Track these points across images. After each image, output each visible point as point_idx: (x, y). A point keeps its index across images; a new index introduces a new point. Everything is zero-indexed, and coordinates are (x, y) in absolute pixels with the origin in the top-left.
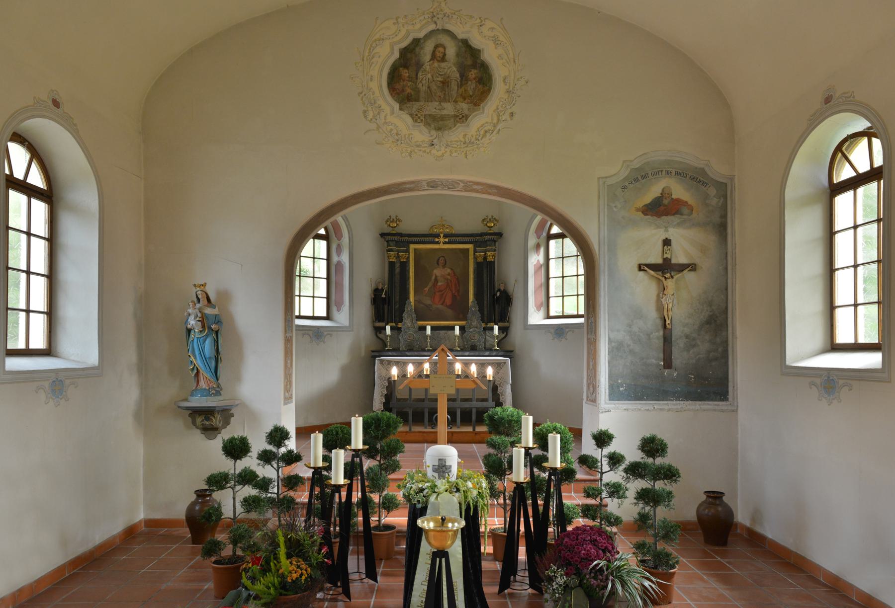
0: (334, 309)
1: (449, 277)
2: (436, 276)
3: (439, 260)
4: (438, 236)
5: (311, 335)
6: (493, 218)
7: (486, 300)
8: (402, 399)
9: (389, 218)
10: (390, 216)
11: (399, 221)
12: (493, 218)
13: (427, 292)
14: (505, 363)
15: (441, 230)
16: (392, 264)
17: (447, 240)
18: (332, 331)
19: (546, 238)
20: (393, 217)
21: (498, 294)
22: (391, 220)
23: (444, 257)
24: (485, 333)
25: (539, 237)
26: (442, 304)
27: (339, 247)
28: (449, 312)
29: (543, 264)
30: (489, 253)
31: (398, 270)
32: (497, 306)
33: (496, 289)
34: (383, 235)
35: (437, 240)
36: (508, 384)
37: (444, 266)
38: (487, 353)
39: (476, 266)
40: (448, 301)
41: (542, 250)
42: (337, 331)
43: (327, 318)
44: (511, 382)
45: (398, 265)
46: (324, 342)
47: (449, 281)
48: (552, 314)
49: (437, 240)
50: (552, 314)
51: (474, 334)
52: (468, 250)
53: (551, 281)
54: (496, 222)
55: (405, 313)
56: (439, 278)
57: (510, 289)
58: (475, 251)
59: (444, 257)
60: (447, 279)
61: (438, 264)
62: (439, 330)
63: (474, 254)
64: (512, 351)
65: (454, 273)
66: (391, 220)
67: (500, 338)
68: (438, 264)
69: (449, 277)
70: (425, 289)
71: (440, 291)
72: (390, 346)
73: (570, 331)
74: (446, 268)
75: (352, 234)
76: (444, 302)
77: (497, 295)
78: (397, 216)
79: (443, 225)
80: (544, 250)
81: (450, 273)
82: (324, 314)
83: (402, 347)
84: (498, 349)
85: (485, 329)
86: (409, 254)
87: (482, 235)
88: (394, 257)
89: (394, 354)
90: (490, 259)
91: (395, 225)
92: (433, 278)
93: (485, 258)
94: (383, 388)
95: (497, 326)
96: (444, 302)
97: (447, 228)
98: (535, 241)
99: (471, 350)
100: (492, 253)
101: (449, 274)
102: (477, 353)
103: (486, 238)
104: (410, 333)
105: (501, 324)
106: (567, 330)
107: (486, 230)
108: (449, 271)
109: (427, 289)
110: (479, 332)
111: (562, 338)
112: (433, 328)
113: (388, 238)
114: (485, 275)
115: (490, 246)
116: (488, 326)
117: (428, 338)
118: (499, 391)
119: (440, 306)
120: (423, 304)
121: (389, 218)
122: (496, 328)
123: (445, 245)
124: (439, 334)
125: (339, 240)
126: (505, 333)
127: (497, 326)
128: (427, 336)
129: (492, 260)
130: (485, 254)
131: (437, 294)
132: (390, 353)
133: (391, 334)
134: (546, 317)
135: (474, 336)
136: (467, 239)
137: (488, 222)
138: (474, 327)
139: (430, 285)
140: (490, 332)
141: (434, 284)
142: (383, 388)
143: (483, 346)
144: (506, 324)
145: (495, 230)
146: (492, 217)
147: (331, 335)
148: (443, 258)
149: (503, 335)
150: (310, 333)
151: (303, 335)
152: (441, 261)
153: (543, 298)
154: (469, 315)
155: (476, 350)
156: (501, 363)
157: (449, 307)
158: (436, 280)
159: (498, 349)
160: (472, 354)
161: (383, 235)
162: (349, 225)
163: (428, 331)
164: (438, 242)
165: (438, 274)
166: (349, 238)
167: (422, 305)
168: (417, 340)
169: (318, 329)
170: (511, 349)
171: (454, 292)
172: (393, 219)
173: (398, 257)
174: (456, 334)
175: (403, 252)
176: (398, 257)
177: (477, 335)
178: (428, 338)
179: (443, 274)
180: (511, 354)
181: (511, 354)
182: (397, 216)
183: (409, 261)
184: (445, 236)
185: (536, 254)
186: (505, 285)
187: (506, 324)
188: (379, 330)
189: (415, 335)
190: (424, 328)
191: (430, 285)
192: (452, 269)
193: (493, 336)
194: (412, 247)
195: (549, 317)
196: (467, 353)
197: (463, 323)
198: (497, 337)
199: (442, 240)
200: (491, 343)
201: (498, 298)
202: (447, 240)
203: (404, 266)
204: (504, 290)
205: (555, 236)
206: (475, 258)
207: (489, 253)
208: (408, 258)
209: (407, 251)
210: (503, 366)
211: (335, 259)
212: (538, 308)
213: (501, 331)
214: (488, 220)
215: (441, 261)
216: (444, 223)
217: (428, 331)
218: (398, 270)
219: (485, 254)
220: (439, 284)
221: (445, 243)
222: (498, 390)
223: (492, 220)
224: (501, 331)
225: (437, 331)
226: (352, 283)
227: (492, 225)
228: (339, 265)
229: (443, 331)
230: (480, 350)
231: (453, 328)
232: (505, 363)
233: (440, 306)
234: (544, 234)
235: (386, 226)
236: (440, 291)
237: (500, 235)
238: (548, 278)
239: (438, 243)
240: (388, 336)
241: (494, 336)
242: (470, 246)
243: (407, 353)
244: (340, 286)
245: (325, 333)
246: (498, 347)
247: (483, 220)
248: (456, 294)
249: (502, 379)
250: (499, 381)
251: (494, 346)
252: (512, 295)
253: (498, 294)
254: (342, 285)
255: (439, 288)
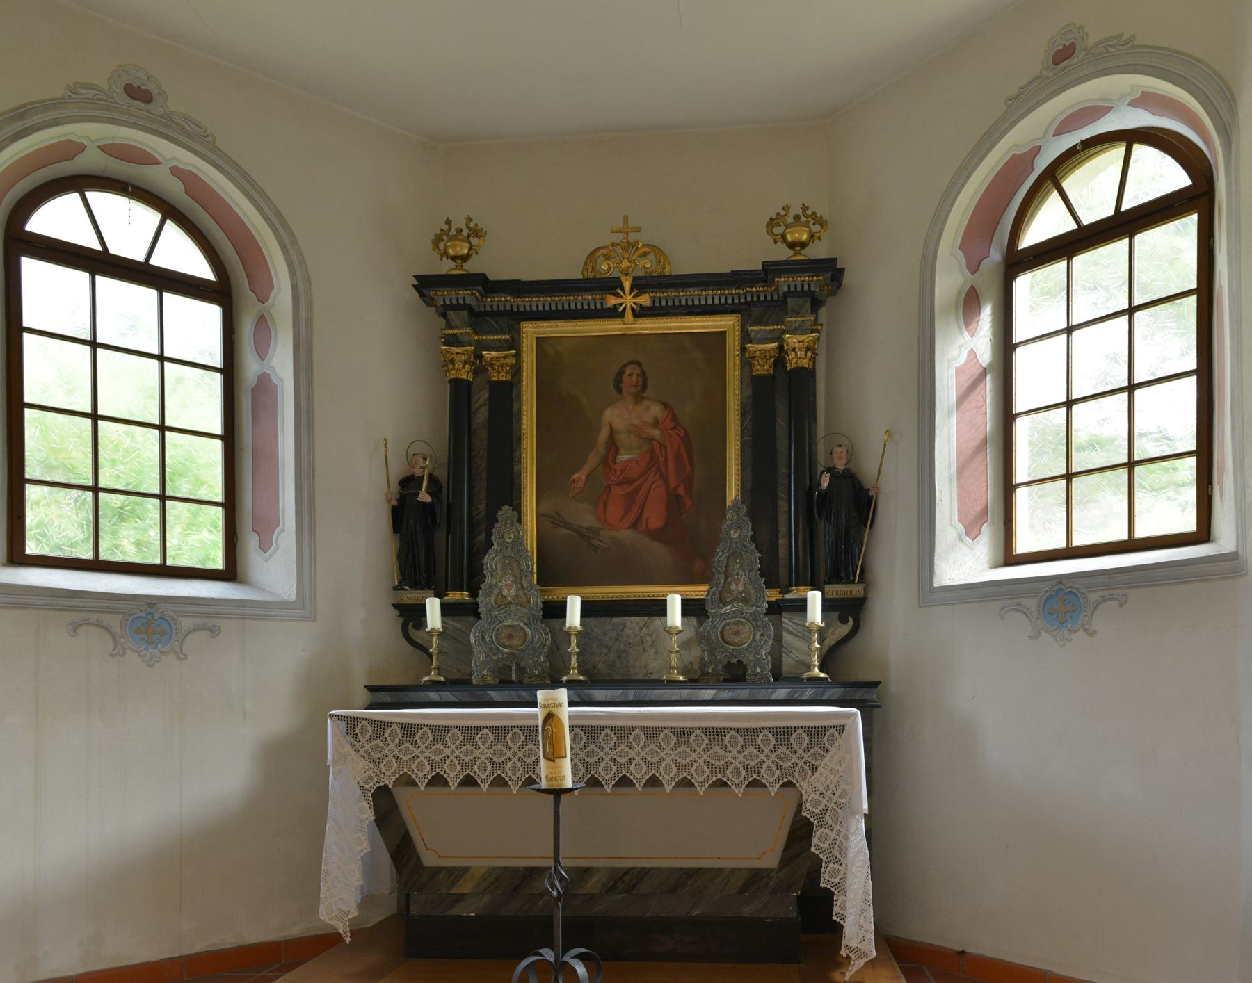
0: (250, 542)
1: (656, 433)
2: (612, 432)
3: (621, 373)
4: (612, 285)
5: (116, 628)
6: (809, 212)
7: (787, 507)
8: (442, 868)
9: (446, 227)
10: (448, 222)
11: (477, 232)
12: (809, 212)
13: (581, 484)
14: (841, 729)
15: (625, 264)
16: (460, 393)
17: (645, 300)
18: (219, 616)
19: (1002, 269)
20: (459, 223)
21: (825, 482)
22: (453, 232)
23: (638, 364)
24: (779, 628)
25: (974, 267)
26: (634, 526)
27: (263, 323)
28: (659, 552)
29: (991, 364)
30: (791, 340)
31: (481, 415)
32: (821, 525)
33: (820, 469)
34: (425, 284)
35: (611, 301)
36: (853, 814)
37: (639, 397)
38: (782, 693)
39: (749, 392)
40: (655, 517)
41: (986, 316)
42: (243, 617)
43: (230, 572)
44: (865, 806)
45: (481, 398)
46: (183, 657)
47: (656, 445)
48: (1022, 545)
49: (611, 301)
50: (1022, 545)
51: (737, 623)
52: (722, 335)
53: (1022, 427)
54: (816, 228)
55: (491, 551)
56: (621, 438)
57: (868, 469)
58: (746, 338)
59: (638, 364)
60: (650, 440)
61: (619, 390)
62: (622, 616)
63: (743, 349)
64: (875, 684)
65: (674, 418)
66: (453, 232)
67: (832, 639)
68: (619, 390)
69: (656, 433)
70: (576, 476)
71: (627, 481)
72: (438, 668)
73: (1111, 598)
74: (646, 403)
75: (308, 279)
76: (639, 518)
77: (820, 484)
78: (469, 219)
79: (630, 246)
80: (993, 314)
81: (660, 417)
82: (217, 562)
83: (480, 672)
84: (823, 675)
85: (776, 609)
86: (518, 356)
87: (771, 270)
88: (465, 363)
89: (448, 696)
90: (797, 359)
91: (465, 251)
92: (603, 435)
93: (780, 359)
94: (746, 767)
95: (818, 594)
96: (639, 518)
97: (644, 255)
98: (961, 280)
99: (726, 680)
100: (803, 337)
101: (656, 423)
102: (744, 693)
103: (784, 282)
104: (509, 622)
105: (837, 590)
106: (1094, 596)
107: (782, 253)
108: (656, 411)
109: (580, 476)
110: (755, 616)
111: (1071, 631)
112: (588, 609)
113: (445, 296)
114: (781, 423)
115: (797, 313)
116: (791, 596)
117: (574, 641)
118: (818, 843)
119: (626, 534)
120: (567, 525)
121: (446, 227)
122: (815, 599)
123: (640, 320)
124: (624, 626)
125: (262, 300)
126: (851, 622)
127: (818, 594)
128: (567, 635)
129: (805, 364)
130: (781, 348)
131: (618, 491)
132: (434, 696)
133: (443, 627)
134: (1002, 560)
135: (737, 633)
136: (712, 296)
137: (787, 226)
138: (736, 599)
139: (593, 460)
140: (797, 618)
141: (607, 457)
142: (746, 767)
143: (769, 667)
144: (854, 590)
145: (818, 251)
146: (805, 208)
147: (214, 631)
148: (637, 370)
149: (844, 630)
150: (109, 619)
151: (75, 627)
152: (631, 377)
153: (988, 490)
154: (721, 556)
155: (745, 681)
156: (825, 729)
157: (656, 535)
158: (613, 446)
159: (823, 675)
160: (726, 695)
161: (425, 284)
162: (294, 242)
163: (574, 617)
164: (615, 307)
165: (619, 424)
166: (295, 289)
167: (565, 531)
168: (535, 650)
169: (151, 605)
170: (872, 678)
171: (673, 484)
172: (460, 231)
173: (479, 366)
174: (669, 624)
175: (497, 350)
176: (479, 366)
177: (747, 629)
178: (574, 641)
179: (635, 421)
180: (872, 695)
181: (872, 695)
182: (469, 219)
183: (520, 382)
184: (641, 285)
185: (966, 334)
186: (851, 454)
187: (854, 590)
188: (413, 615)
189: (528, 631)
190: (556, 610)
191: (593, 460)
192: (666, 406)
193: (805, 632)
194: (530, 331)
195: (1011, 559)
196: (708, 694)
197: (699, 590)
198: (821, 631)
199: (629, 300)
200: (801, 657)
201: (824, 496)
202: (645, 300)
203: (505, 395)
204: (847, 470)
205: (1035, 257)
206: (746, 362)
207: (791, 340)
208: (517, 370)
209: (514, 344)
210: (833, 740)
211: (251, 367)
212: (972, 529)
213: (836, 615)
214: (790, 219)
215: (631, 377)
216: (633, 237)
217: (574, 617)
218: (481, 415)
219: (781, 348)
220: (624, 457)
221: (641, 313)
222: (815, 841)
223: (803, 219)
224: (836, 615)
225: (616, 620)
226: (311, 448)
227: (805, 237)
228: (265, 385)
229: (638, 619)
230: (758, 682)
231: (659, 608)
232: (841, 729)
233: (626, 534)
234: (996, 255)
235: (436, 256)
236: (627, 481)
237: (832, 271)
238: (1007, 417)
239: (614, 313)
240: (430, 633)
241: (810, 631)
242: (727, 323)
243: (495, 695)
244: (267, 457)
245: (186, 623)
246: (821, 670)
247: (772, 223)
248: (681, 491)
249: (828, 795)
250: (815, 803)
251: (809, 667)
252: (876, 486)
253: (825, 482)
254: (273, 458)
255: (622, 471)
